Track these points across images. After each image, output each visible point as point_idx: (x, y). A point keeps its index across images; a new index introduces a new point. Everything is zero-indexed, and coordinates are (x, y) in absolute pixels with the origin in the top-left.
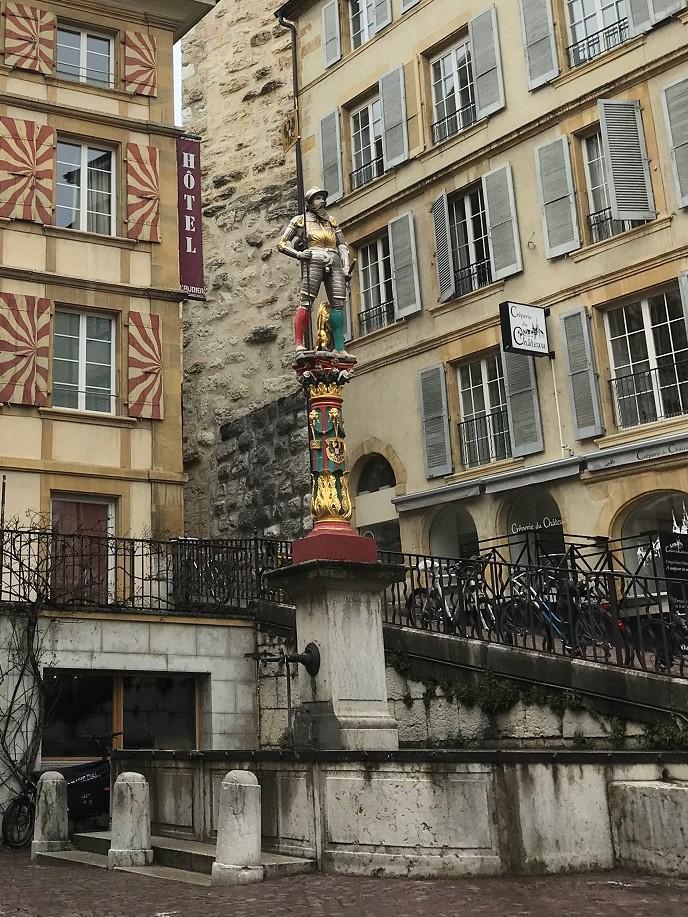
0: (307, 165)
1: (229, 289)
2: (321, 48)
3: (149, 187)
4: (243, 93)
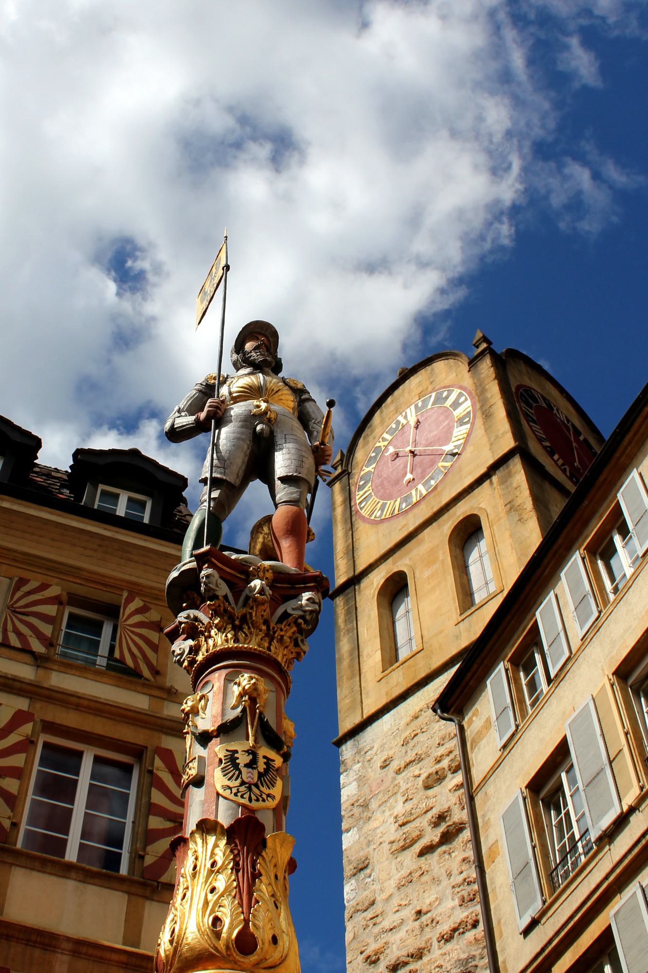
0: (492, 883)
4: (417, 847)
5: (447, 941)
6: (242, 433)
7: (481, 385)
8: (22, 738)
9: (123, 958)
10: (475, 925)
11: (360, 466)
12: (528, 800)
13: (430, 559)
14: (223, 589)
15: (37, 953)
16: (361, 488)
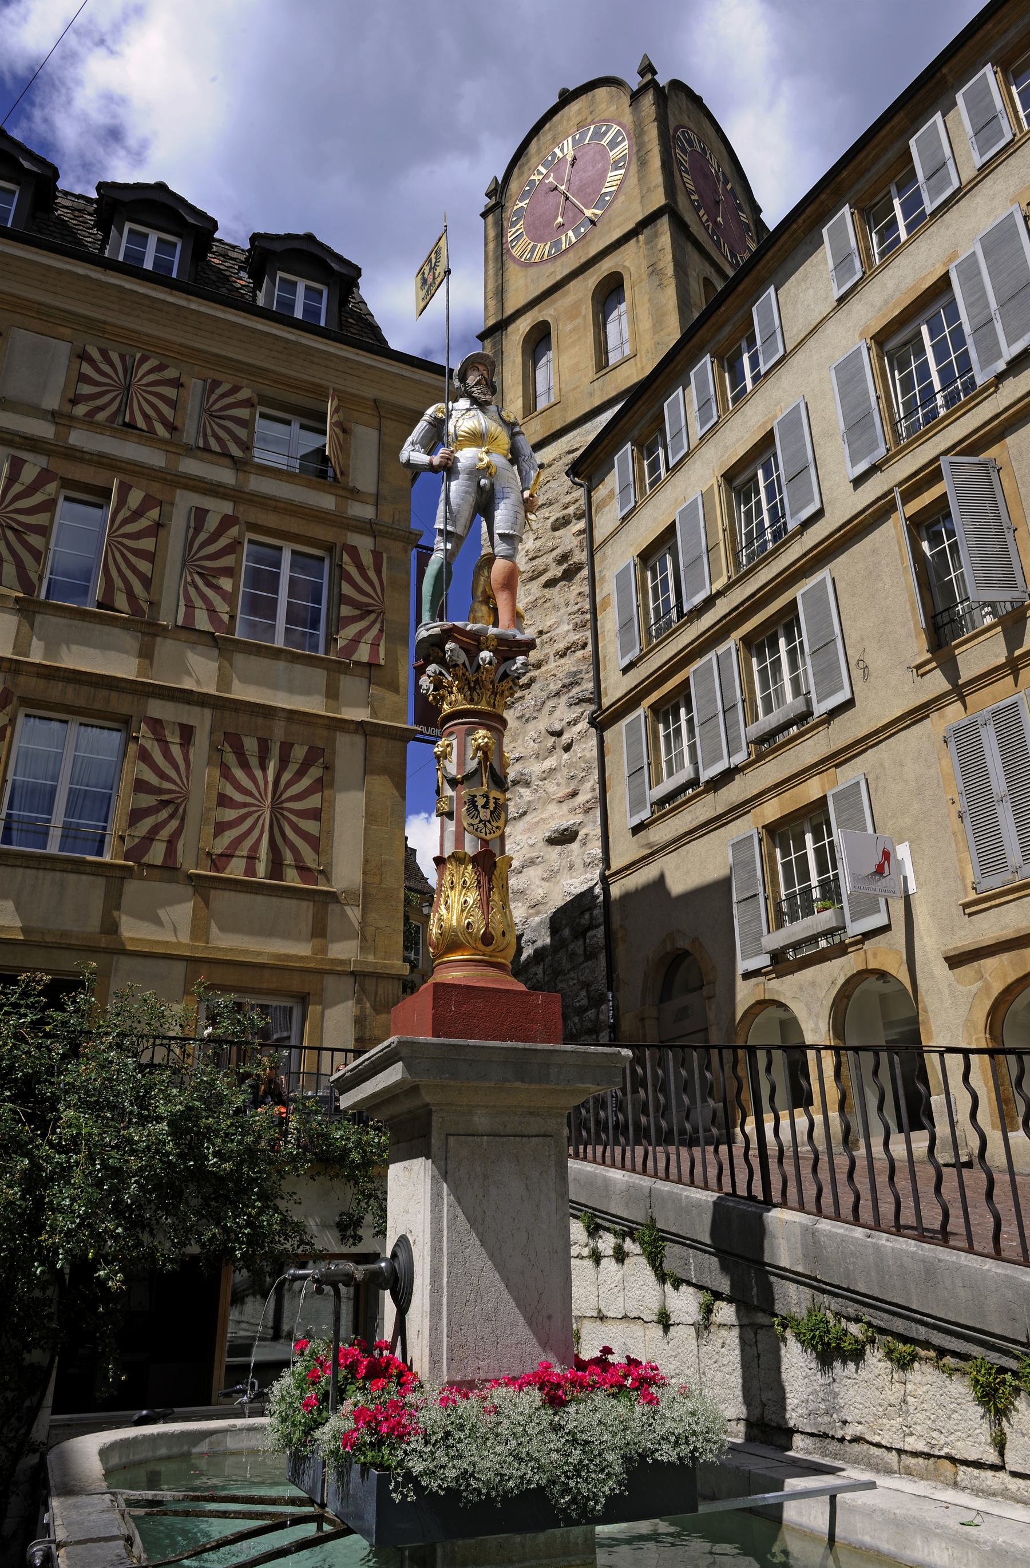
0: (602, 627)
1: (527, 784)
2: (615, 500)
3: (373, 598)
4: (543, 579)
5: (562, 656)
6: (469, 486)
7: (640, 125)
8: (230, 541)
9: (326, 722)
10: (584, 646)
11: (514, 199)
12: (638, 567)
13: (573, 312)
14: (462, 658)
15: (260, 720)
16: (513, 224)
